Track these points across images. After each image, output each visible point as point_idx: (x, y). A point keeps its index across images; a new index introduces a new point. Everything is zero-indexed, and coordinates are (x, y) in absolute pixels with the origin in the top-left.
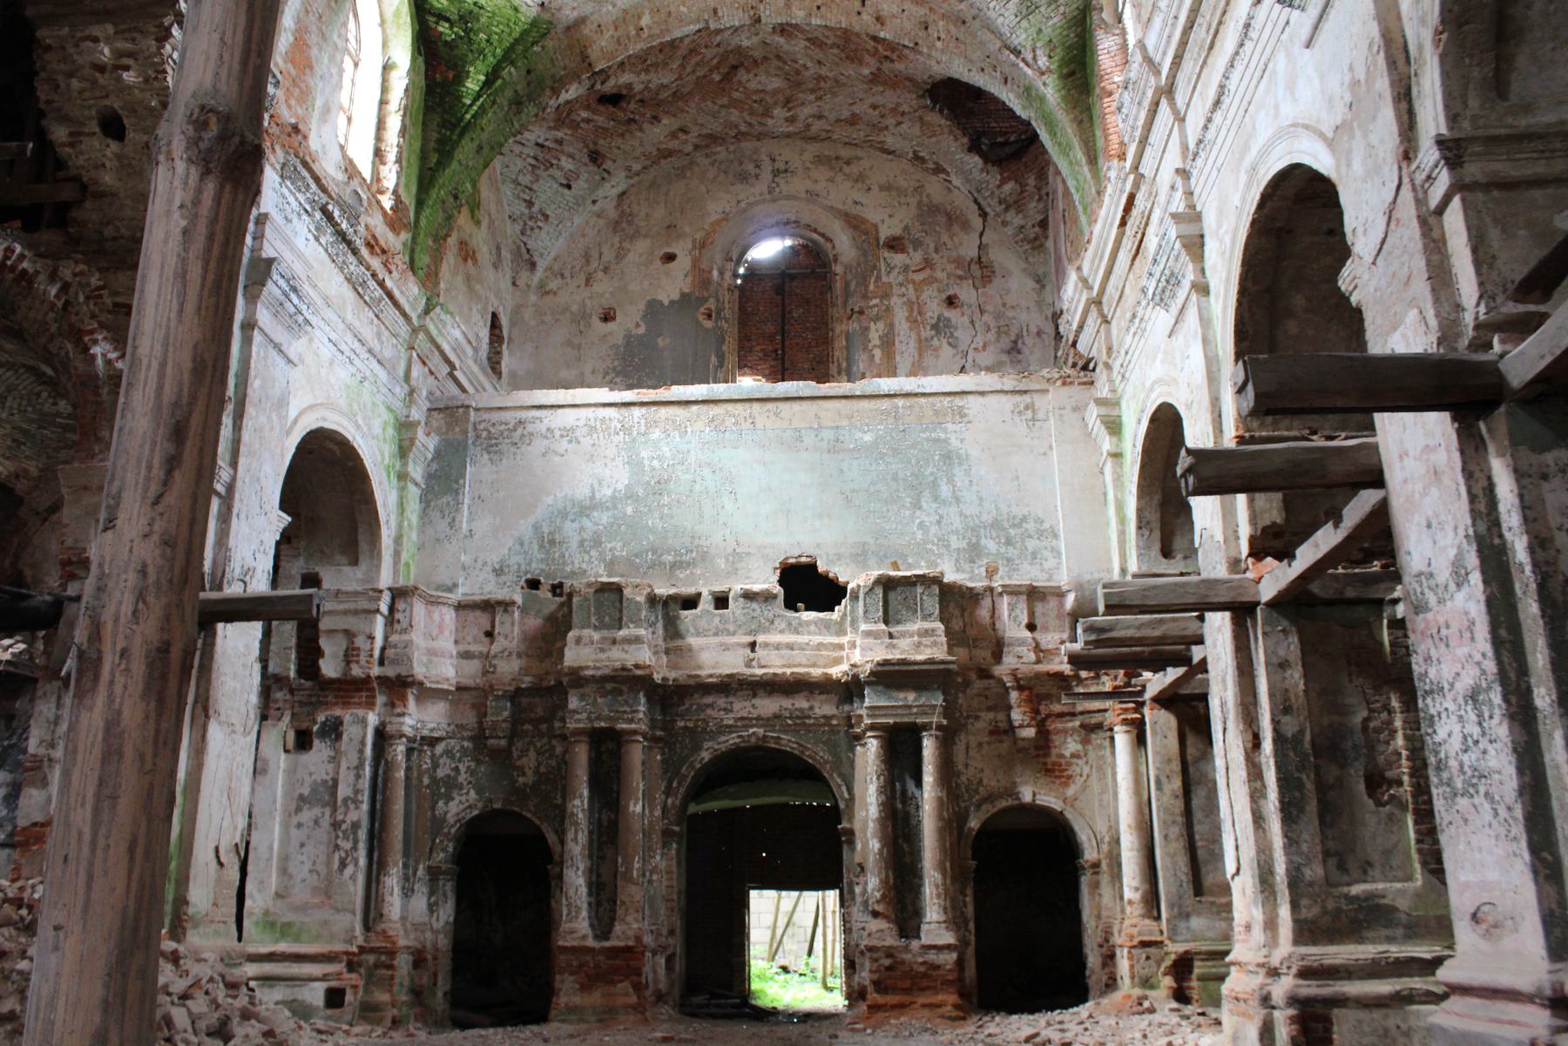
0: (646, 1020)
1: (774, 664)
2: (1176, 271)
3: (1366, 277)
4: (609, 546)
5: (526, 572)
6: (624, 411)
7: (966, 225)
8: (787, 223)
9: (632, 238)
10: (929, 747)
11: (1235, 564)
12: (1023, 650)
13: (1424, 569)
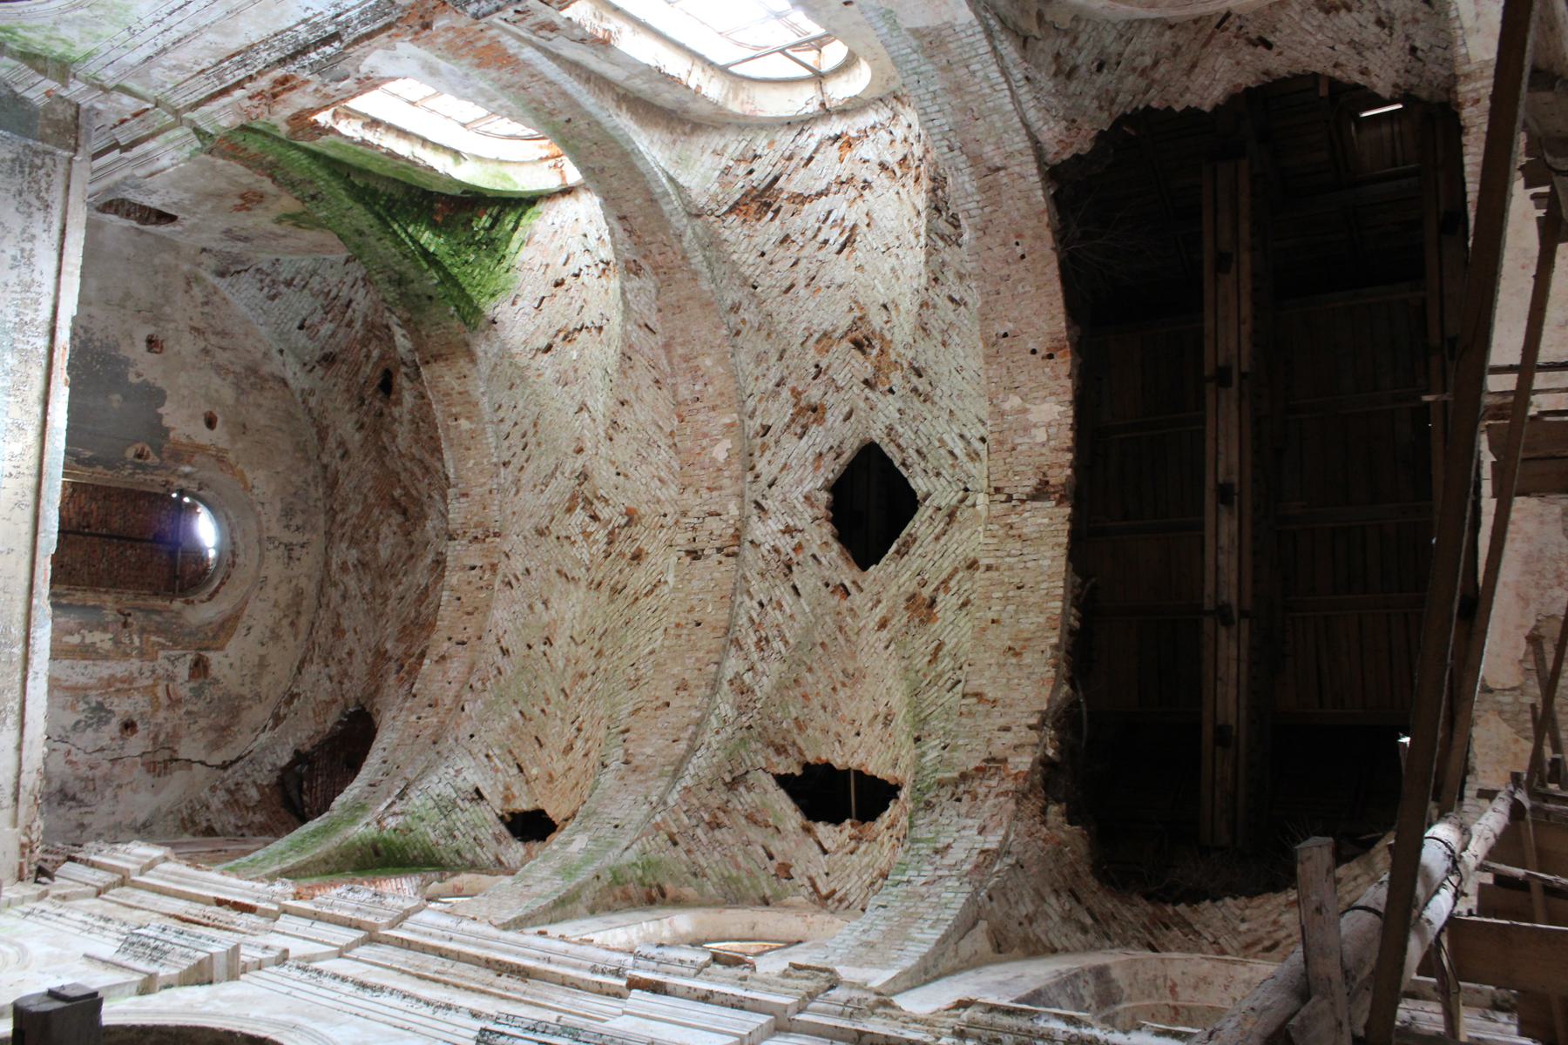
2: (169, 956)
6: (45, 328)
7: (215, 746)
8: (234, 554)
9: (237, 385)
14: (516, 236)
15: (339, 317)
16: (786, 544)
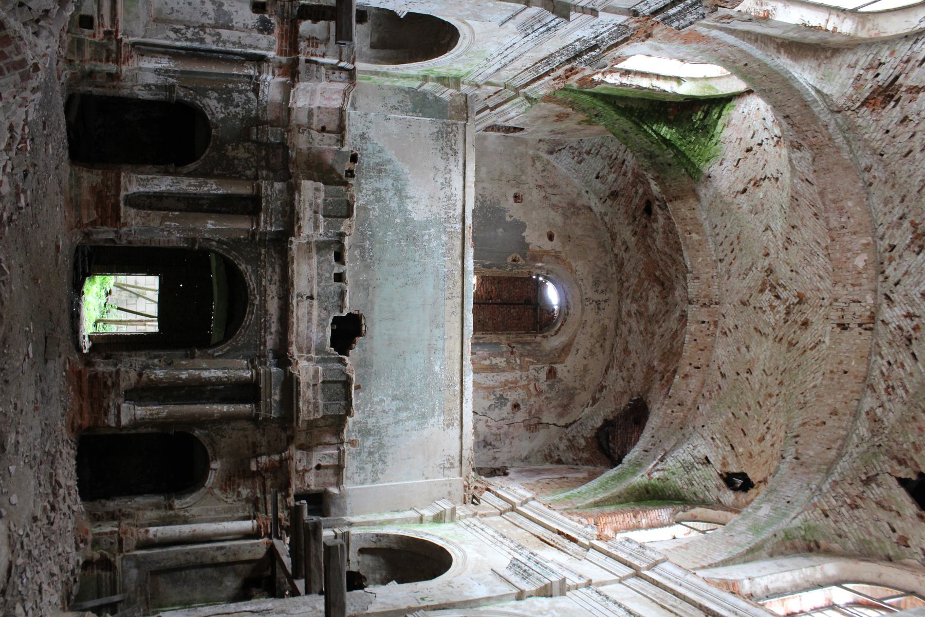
1: (299, 310)
2: (531, 577)
5: (362, 155)
6: (459, 218)
7: (561, 415)
8: (568, 307)
9: (564, 215)
10: (247, 408)
12: (304, 463)
14: (720, 122)
16: (907, 325)
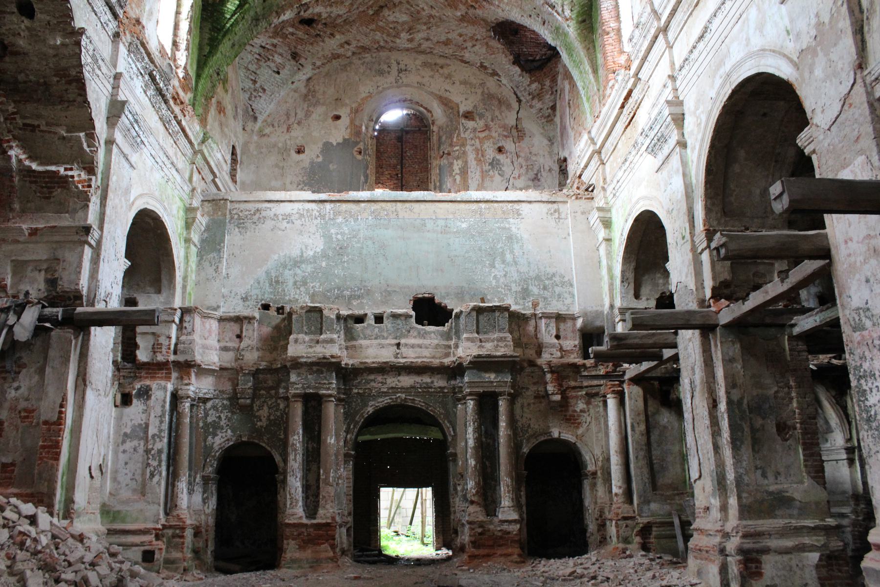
0: (339, 566)
2: (665, 134)
3: (821, 137)
4: (312, 285)
6: (321, 205)
7: (509, 107)
11: (702, 302)
13: (863, 305)
15: (271, 52)
